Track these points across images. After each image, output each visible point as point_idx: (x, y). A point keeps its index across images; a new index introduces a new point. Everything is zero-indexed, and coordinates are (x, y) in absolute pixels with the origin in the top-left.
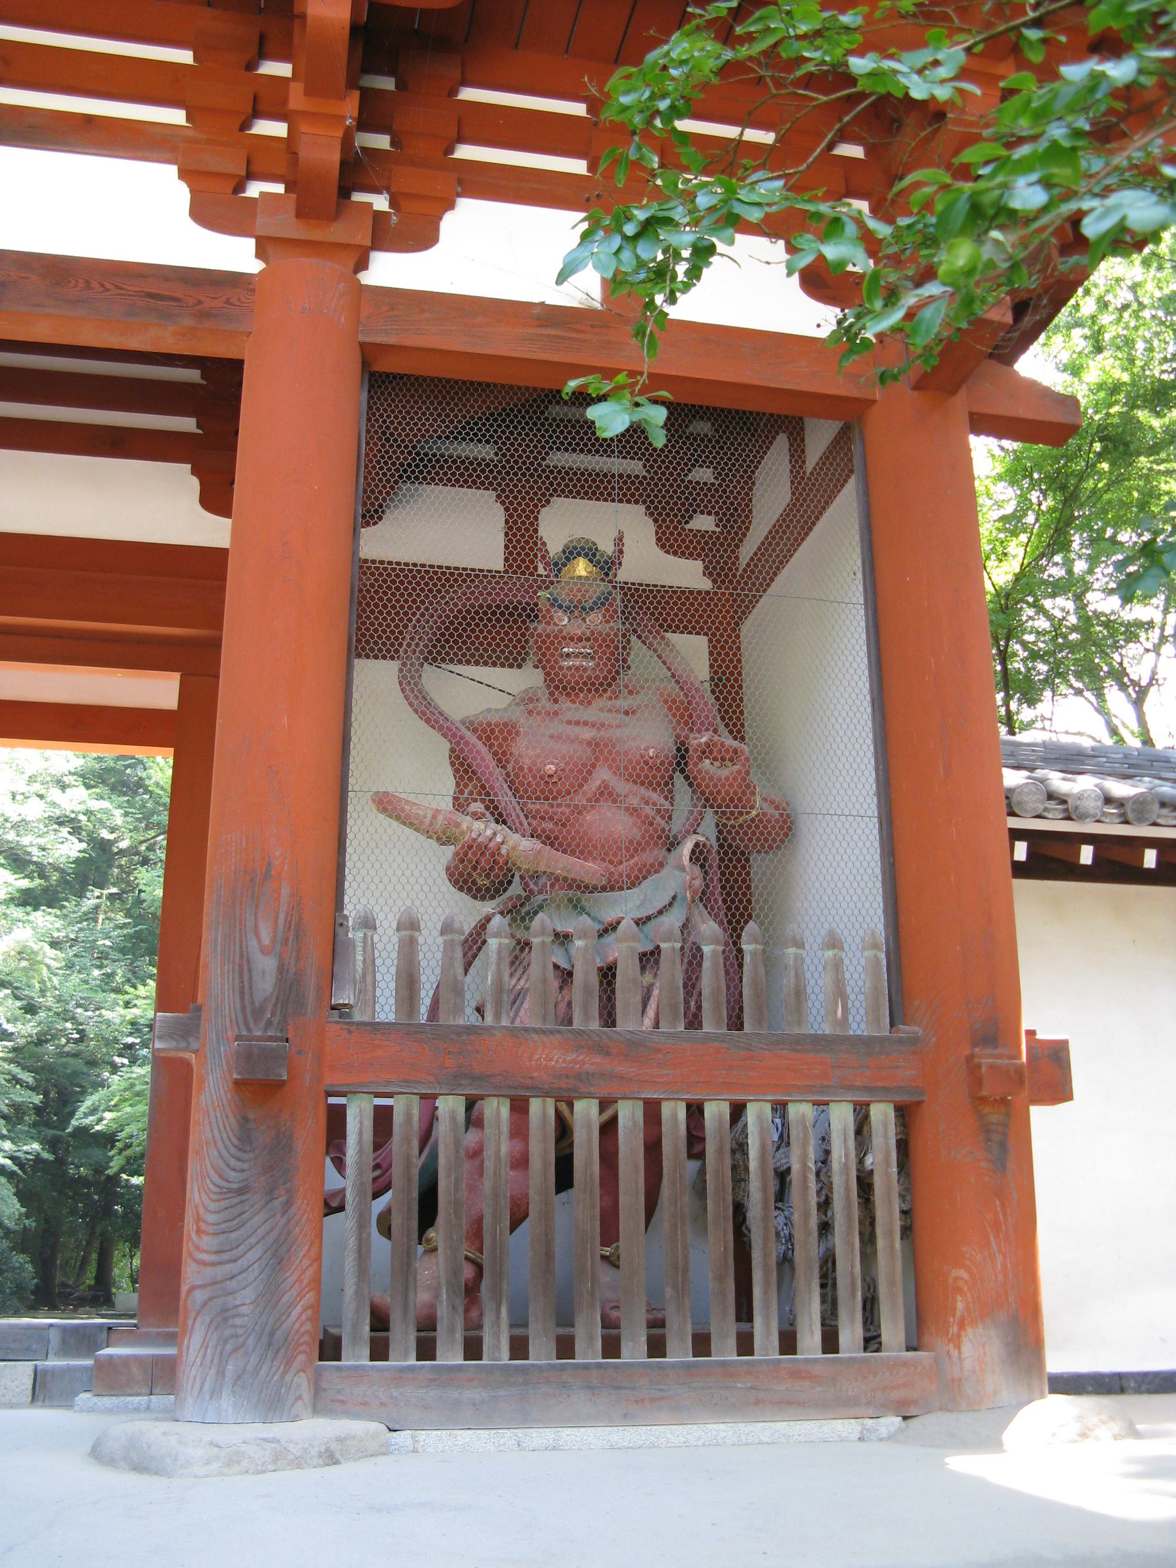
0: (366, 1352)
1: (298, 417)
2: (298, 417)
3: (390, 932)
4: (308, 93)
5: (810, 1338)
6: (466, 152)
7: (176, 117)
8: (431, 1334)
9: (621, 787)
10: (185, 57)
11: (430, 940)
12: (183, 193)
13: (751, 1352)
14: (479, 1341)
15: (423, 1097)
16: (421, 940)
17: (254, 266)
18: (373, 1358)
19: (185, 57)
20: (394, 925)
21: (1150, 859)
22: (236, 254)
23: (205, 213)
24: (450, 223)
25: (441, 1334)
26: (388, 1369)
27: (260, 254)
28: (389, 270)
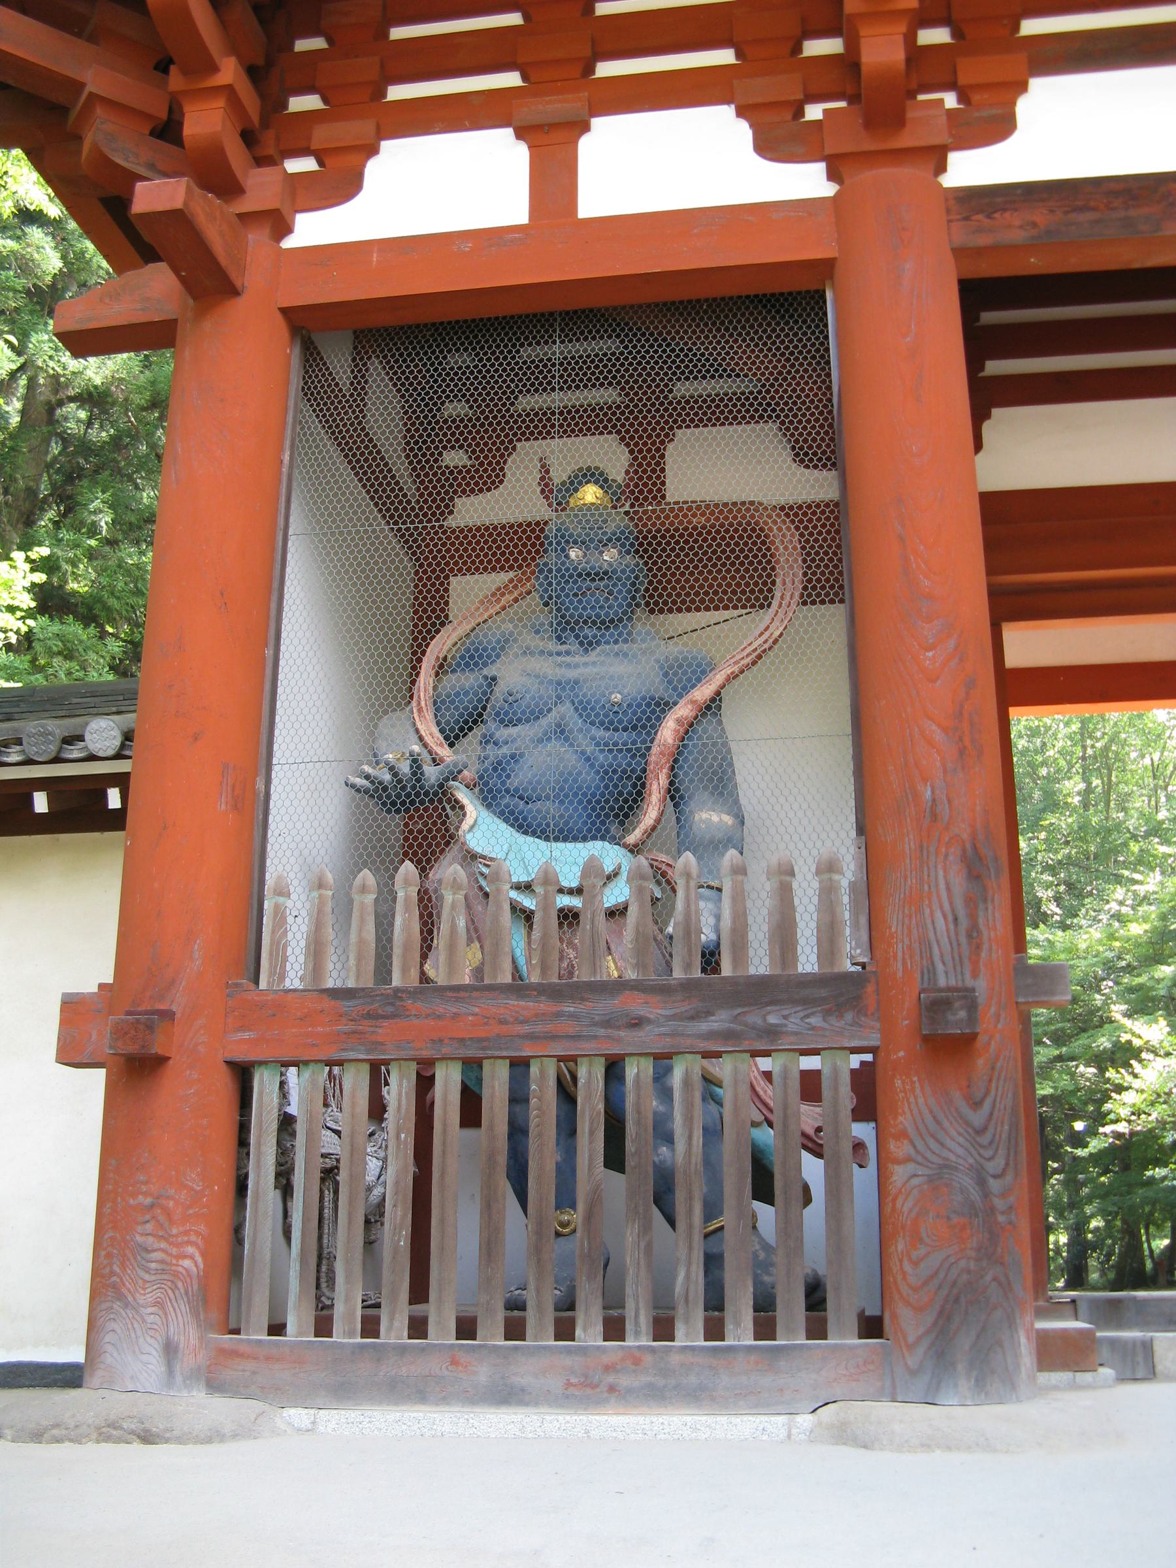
0: (551, 1330)
1: (901, 337)
2: (901, 337)
3: (810, 876)
4: (214, 69)
5: (298, 1321)
6: (1031, 27)
7: (724, 57)
8: (569, 1313)
9: (575, 722)
10: (514, 19)
11: (805, 885)
12: (743, 132)
13: (376, 1335)
14: (621, 1320)
15: (560, 1059)
16: (795, 885)
17: (825, 189)
18: (459, 1337)
19: (514, 19)
20: (813, 869)
21: (41, 803)
22: (807, 181)
23: (770, 146)
24: (1024, 107)
25: (531, 1315)
26: (827, 1346)
27: (832, 175)
28: (968, 169)
